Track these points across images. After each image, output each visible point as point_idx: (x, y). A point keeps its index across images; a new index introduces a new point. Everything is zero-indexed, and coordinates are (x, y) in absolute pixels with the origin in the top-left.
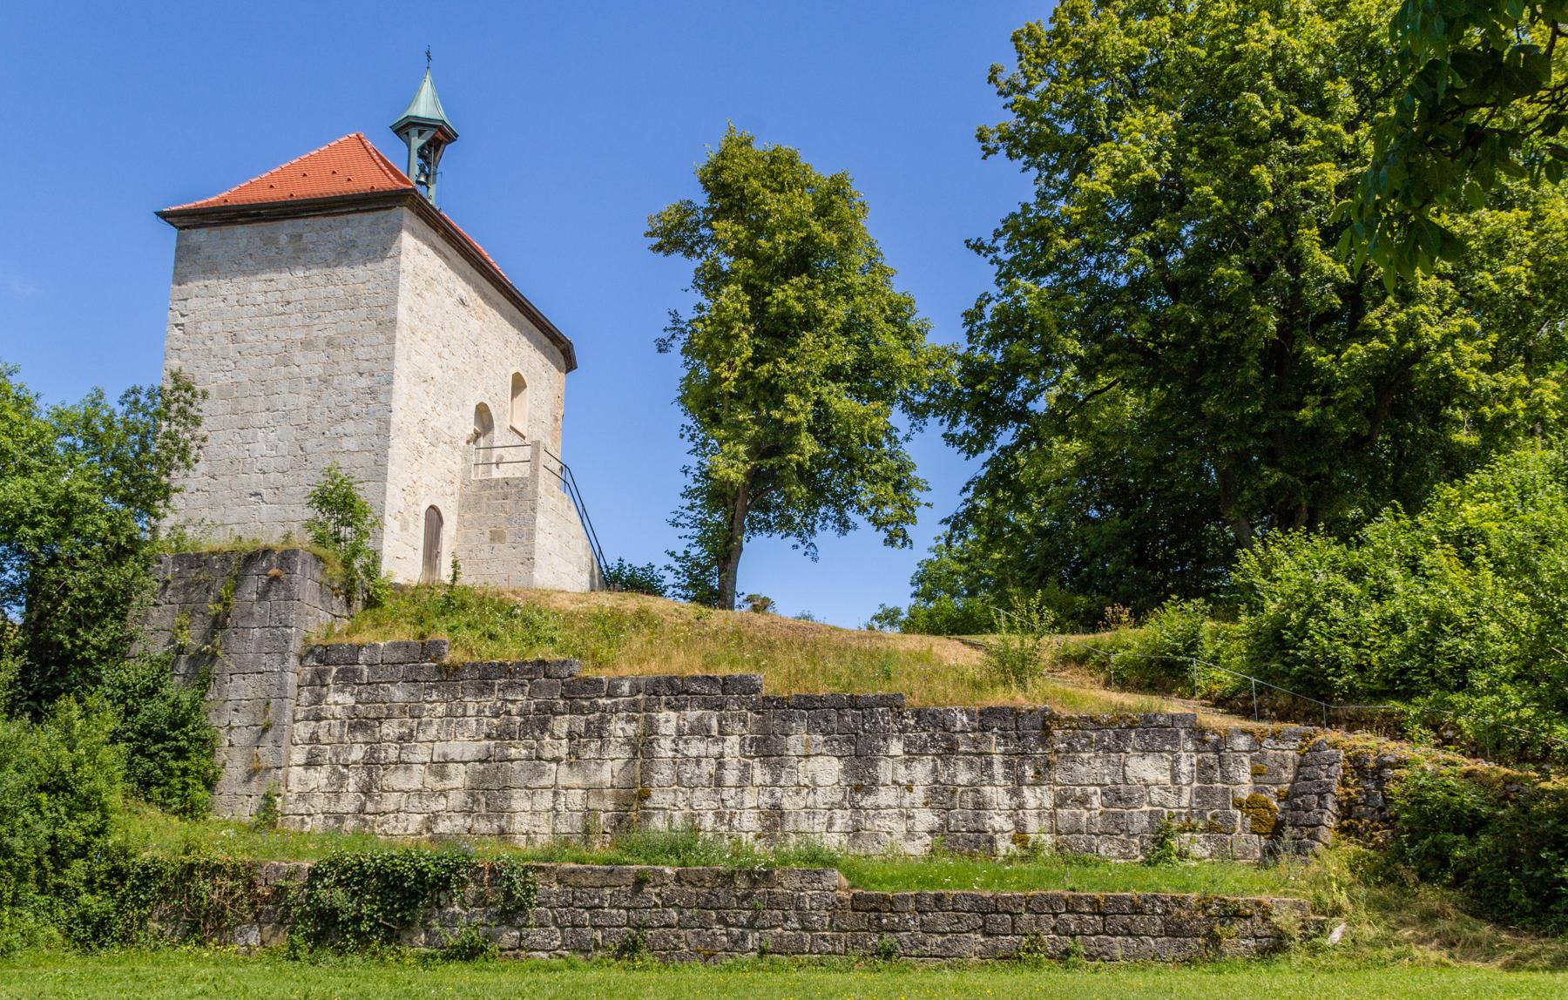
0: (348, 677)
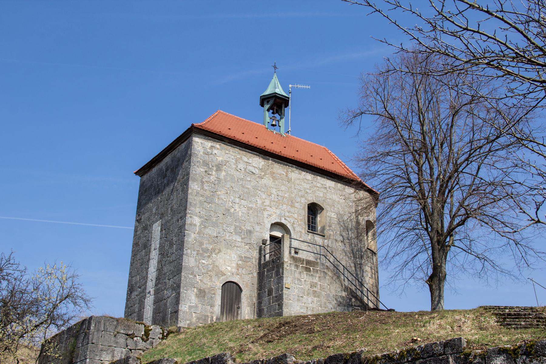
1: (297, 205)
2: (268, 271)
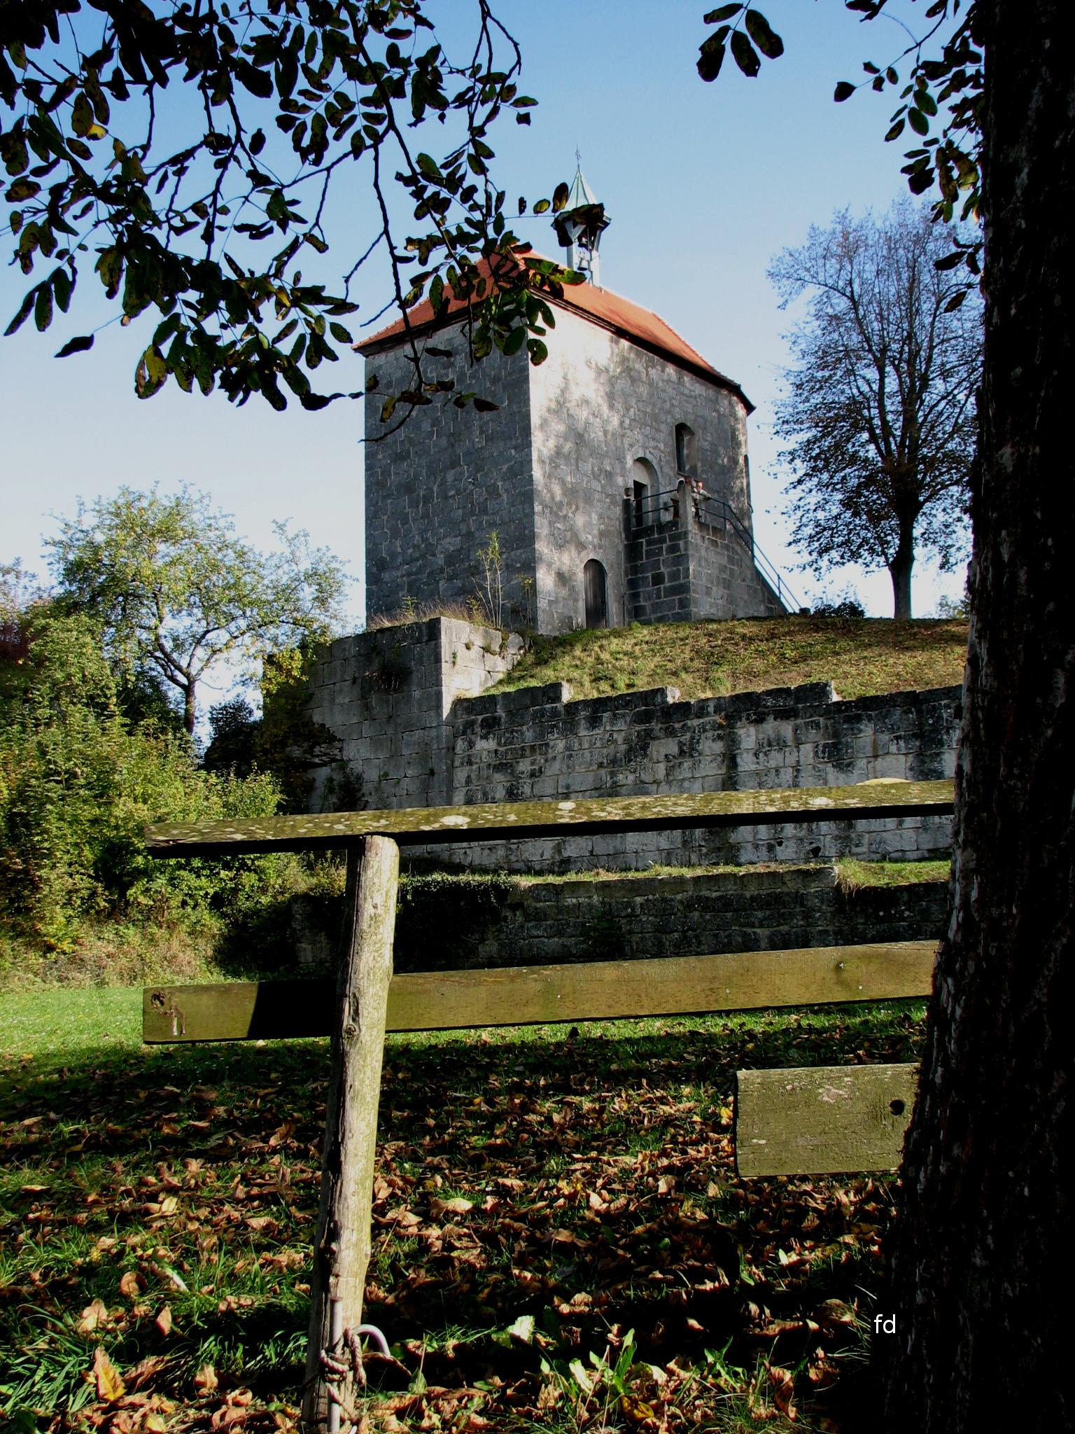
0: (490, 725)
1: (663, 427)
2: (649, 543)
